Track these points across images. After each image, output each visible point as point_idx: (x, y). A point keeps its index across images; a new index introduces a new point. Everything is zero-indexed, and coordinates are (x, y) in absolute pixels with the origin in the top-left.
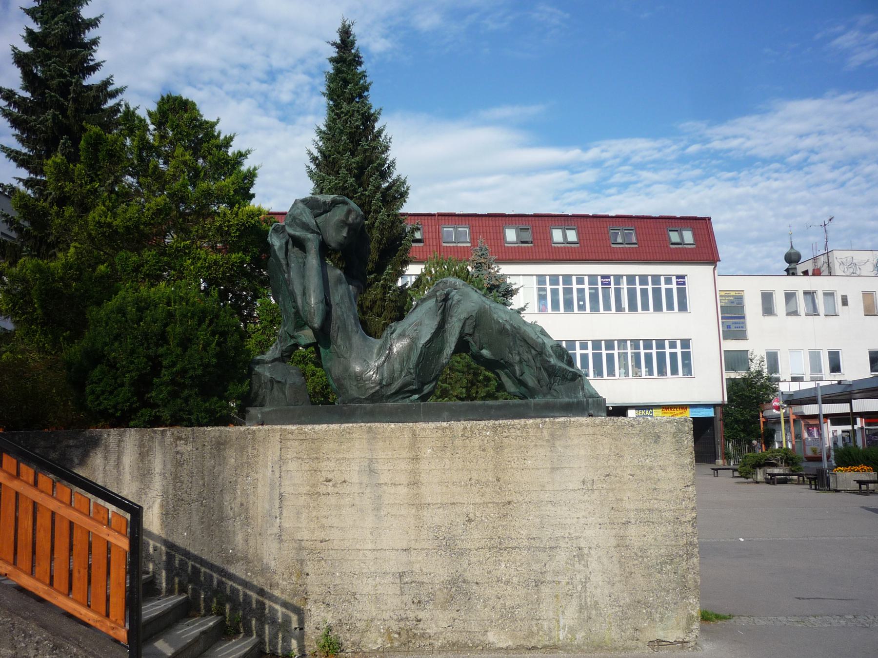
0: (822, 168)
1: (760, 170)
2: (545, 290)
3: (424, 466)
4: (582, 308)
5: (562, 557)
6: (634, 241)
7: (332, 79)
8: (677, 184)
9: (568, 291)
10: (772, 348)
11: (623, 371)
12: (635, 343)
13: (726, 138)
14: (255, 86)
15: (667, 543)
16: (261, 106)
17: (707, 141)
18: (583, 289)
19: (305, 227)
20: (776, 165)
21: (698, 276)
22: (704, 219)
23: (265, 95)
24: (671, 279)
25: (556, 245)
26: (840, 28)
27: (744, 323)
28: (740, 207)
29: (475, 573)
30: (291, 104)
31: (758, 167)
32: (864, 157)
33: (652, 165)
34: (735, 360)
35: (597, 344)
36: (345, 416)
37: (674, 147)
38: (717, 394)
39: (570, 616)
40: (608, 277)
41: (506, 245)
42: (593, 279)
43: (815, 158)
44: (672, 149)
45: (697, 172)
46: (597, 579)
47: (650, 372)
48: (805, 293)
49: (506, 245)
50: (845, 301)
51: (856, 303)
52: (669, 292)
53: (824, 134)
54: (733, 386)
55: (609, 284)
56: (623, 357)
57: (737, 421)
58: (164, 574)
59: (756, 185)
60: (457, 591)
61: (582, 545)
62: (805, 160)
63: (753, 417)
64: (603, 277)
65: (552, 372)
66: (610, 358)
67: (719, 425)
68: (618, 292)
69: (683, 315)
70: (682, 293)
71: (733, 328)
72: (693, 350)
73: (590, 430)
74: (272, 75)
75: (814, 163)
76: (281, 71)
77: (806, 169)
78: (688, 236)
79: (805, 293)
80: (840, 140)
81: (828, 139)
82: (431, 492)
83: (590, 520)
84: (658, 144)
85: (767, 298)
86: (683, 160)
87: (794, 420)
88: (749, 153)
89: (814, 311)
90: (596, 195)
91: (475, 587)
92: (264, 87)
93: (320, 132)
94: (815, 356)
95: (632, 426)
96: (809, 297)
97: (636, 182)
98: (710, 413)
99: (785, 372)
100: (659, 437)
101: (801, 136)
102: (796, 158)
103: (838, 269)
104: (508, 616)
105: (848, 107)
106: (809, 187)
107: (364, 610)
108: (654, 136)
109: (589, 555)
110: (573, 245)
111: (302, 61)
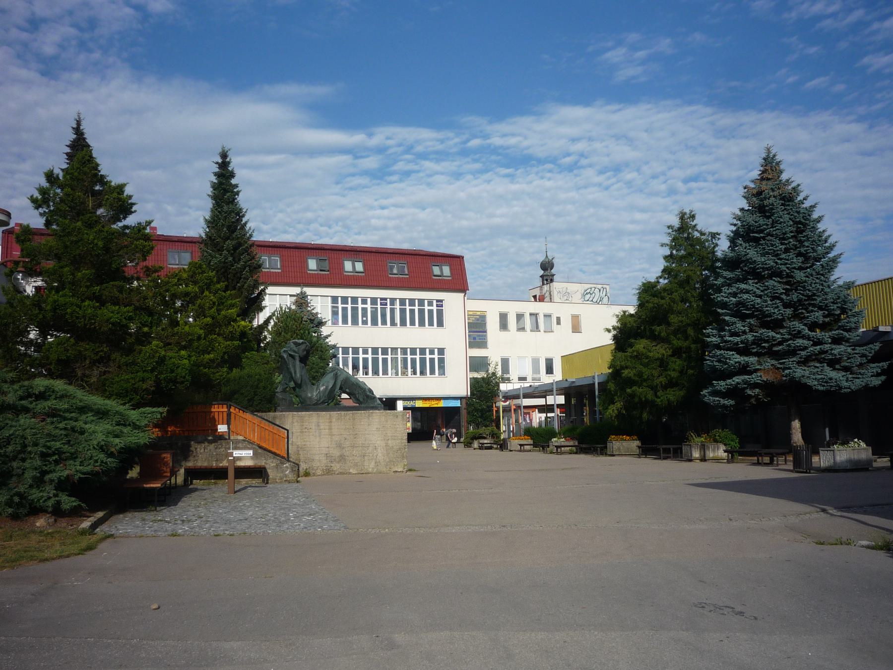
0: (589, 173)
1: (535, 169)
2: (337, 307)
3: (333, 424)
4: (365, 322)
5: (371, 449)
6: (406, 272)
7: (215, 187)
8: (457, 175)
9: (355, 310)
10: (505, 355)
11: (394, 371)
12: (404, 351)
13: (504, 135)
14: (14, 33)
16: (19, 56)
17: (486, 136)
19: (294, 351)
20: (549, 166)
21: (452, 301)
23: (25, 45)
26: (610, 44)
27: (486, 336)
28: (515, 202)
29: (347, 454)
30: (55, 58)
31: (533, 166)
32: (627, 164)
33: (434, 156)
34: (477, 364)
35: (375, 351)
36: (307, 410)
37: (457, 140)
38: (462, 389)
39: (373, 464)
40: (386, 299)
42: (374, 301)
43: (584, 162)
44: (453, 140)
45: (478, 166)
46: (380, 455)
47: (415, 373)
48: (531, 314)
50: (559, 321)
51: (567, 323)
52: (431, 312)
53: (593, 140)
54: (475, 384)
55: (386, 304)
56: (395, 360)
57: (476, 410)
58: (158, 485)
59: (531, 182)
60: (342, 458)
62: (576, 163)
63: (488, 407)
64: (382, 299)
65: (368, 397)
66: (385, 361)
67: (464, 413)
68: (392, 311)
69: (440, 329)
70: (440, 314)
71: (477, 340)
72: (447, 356)
74: (34, 24)
75: (583, 167)
76: (44, 20)
77: (575, 172)
78: (446, 270)
79: (531, 314)
80: (607, 147)
81: (597, 145)
82: (335, 431)
84: (441, 135)
85: (503, 317)
86: (464, 153)
87: (515, 410)
88: (526, 152)
89: (536, 328)
90: (378, 181)
92: (25, 36)
93: (206, 220)
94: (535, 362)
96: (534, 318)
97: (418, 172)
98: (457, 404)
99: (514, 374)
101: (574, 140)
102: (568, 160)
103: (556, 298)
104: (356, 465)
105: (616, 117)
106: (578, 188)
107: (316, 464)
108: (438, 127)
111: (71, 13)
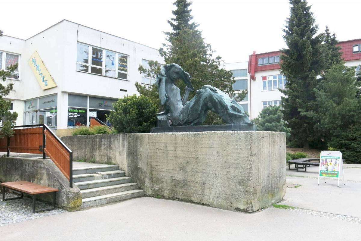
15: (242, 175)
18: (276, 81)
22: (56, 93)
24: (276, 77)
25: (259, 66)
41: (258, 66)
49: (258, 66)
61: (216, 173)
73: (220, 135)
83: (219, 165)
91: (188, 183)
95: (232, 134)
100: (240, 138)
109: (218, 176)
110: (266, 65)
